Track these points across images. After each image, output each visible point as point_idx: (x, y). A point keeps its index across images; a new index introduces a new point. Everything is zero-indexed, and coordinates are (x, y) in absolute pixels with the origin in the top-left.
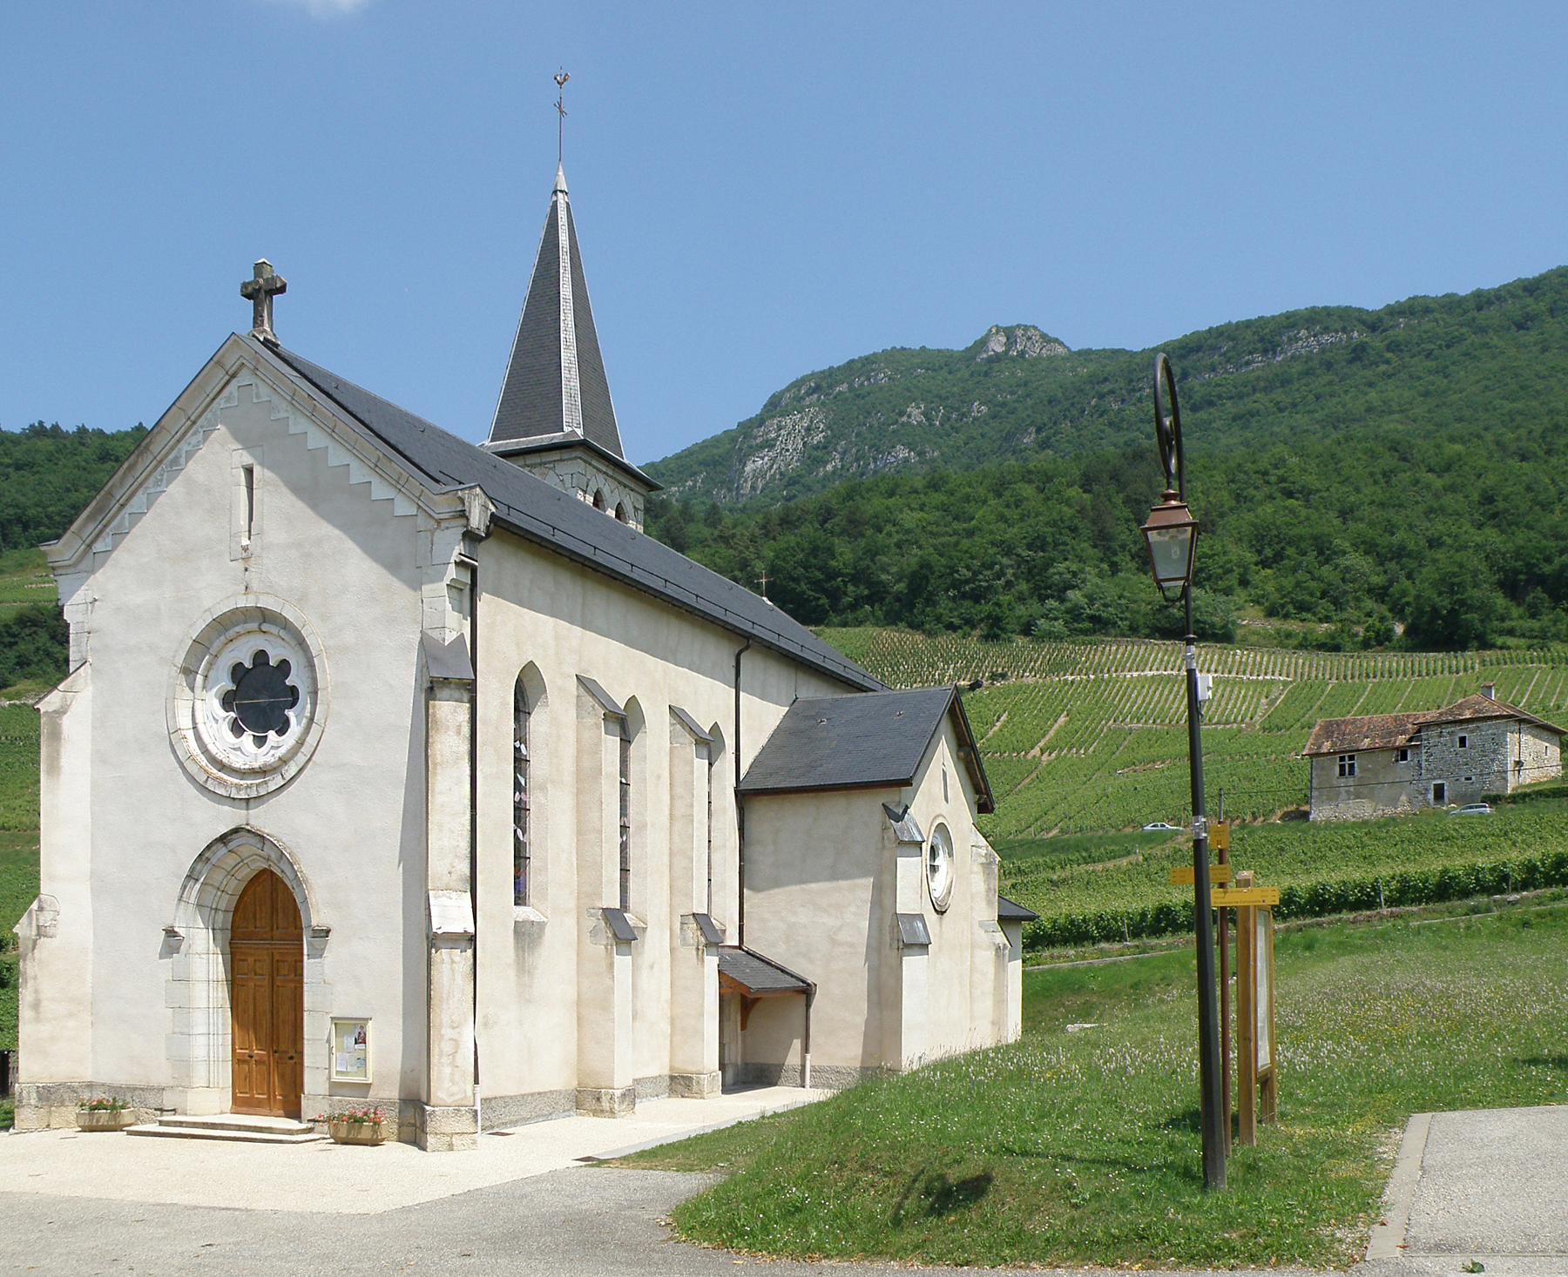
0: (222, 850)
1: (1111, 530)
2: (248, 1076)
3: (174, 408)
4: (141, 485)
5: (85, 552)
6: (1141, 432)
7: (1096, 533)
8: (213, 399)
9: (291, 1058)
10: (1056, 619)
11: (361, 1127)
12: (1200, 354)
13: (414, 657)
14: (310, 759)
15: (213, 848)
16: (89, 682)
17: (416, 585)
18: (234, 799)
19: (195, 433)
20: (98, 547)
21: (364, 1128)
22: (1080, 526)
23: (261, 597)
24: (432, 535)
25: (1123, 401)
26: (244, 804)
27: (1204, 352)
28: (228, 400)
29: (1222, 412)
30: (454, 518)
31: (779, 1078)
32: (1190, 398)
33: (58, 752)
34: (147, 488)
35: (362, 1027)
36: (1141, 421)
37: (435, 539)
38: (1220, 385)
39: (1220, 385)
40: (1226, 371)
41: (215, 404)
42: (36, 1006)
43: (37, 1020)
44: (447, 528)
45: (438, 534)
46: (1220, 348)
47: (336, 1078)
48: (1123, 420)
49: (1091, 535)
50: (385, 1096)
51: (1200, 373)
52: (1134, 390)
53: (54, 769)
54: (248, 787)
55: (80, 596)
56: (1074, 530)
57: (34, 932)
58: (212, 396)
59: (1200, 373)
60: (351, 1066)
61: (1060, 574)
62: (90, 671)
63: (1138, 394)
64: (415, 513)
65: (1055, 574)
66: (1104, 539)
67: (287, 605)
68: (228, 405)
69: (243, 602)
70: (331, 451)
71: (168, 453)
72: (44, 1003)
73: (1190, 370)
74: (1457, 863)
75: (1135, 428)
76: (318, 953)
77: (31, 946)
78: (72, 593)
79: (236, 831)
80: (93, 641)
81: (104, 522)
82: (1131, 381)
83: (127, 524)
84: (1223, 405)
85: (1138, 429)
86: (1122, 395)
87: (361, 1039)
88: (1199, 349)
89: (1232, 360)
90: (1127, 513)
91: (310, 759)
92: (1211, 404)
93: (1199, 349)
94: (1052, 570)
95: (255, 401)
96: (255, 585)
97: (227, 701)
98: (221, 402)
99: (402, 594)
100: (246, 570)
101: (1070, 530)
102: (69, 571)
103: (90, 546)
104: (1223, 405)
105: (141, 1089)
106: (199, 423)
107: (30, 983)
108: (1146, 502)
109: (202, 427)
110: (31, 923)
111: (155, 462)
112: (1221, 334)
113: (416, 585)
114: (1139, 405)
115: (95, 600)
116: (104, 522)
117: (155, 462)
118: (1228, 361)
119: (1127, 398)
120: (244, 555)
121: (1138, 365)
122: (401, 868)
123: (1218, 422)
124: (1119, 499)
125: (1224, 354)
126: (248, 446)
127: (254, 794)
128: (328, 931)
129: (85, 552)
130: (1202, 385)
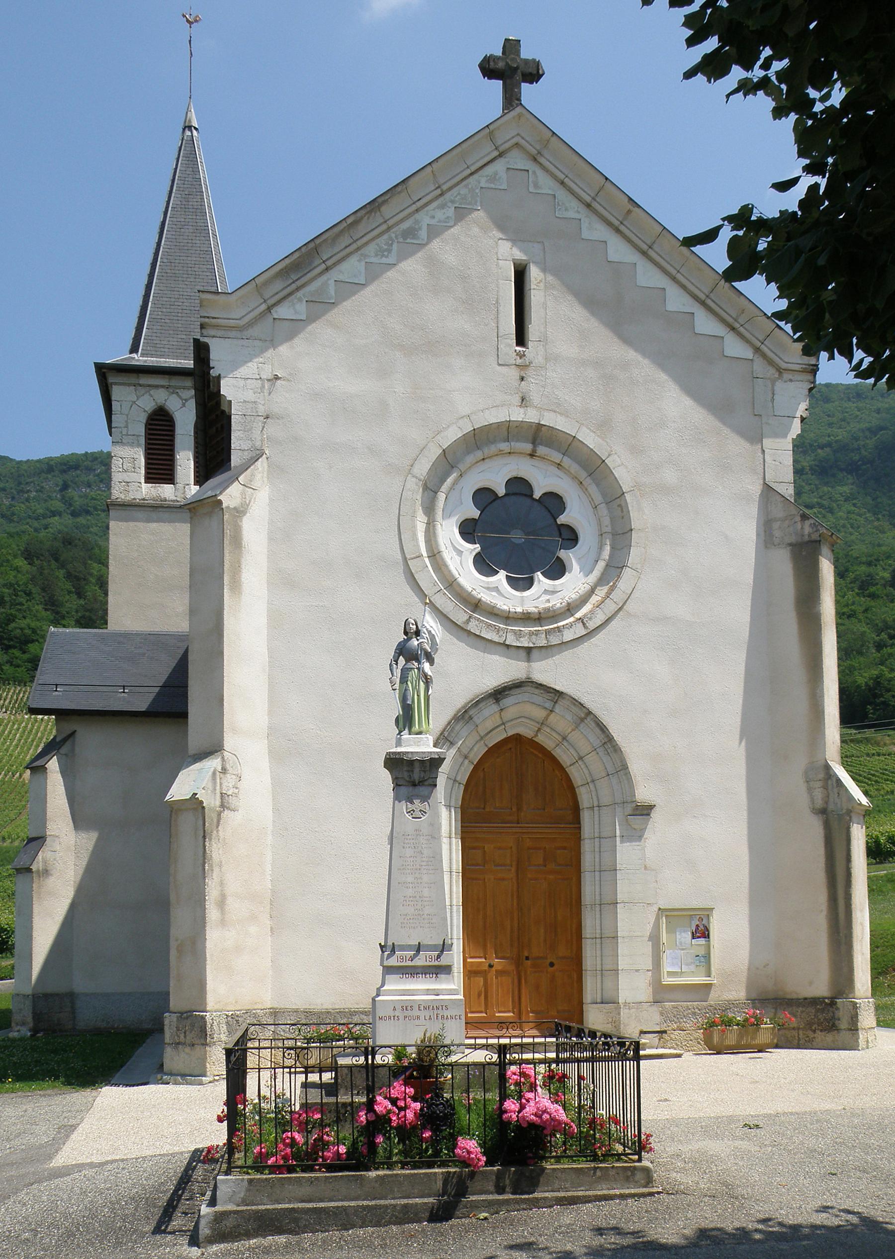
0: (491, 709)
1: (60, 598)
2: (486, 993)
3: (429, 169)
4: (359, 249)
5: (262, 315)
6: (30, 526)
7: (47, 598)
8: (472, 174)
9: (552, 965)
10: (18, 666)
11: (758, 1030)
12: (78, 472)
13: (754, 509)
14: (620, 609)
15: (481, 705)
16: (265, 479)
17: (755, 437)
18: (508, 646)
19: (442, 206)
20: (282, 312)
21: (761, 1032)
22: (34, 591)
23: (546, 414)
24: (773, 385)
25: (13, 498)
26: (523, 654)
27: (81, 471)
28: (493, 178)
29: (98, 520)
30: (804, 371)
31: (144, 1042)
32: (71, 505)
33: (239, 562)
34: (366, 256)
35: (701, 919)
36: (30, 517)
37: (775, 388)
38: (95, 499)
39: (95, 499)
40: (100, 489)
41: (472, 180)
42: (222, 903)
43: (223, 923)
44: (791, 380)
45: (779, 385)
46: (95, 470)
47: (667, 980)
48: (13, 514)
49: (43, 600)
50: (731, 997)
51: (78, 487)
52: (22, 491)
53: (236, 586)
54: (531, 634)
55: (250, 369)
56: (29, 594)
57: (218, 803)
58: (473, 168)
59: (78, 487)
60: (687, 965)
61: (22, 629)
62: (265, 465)
63: (26, 495)
64: (751, 358)
65: (16, 628)
66: (53, 604)
67: (584, 429)
68: (492, 186)
69: (518, 415)
70: (640, 268)
71: (402, 221)
72: (230, 900)
73: (70, 483)
74: (500, 868)
75: (25, 522)
76: (635, 835)
77: (215, 820)
78: (236, 366)
79: (518, 685)
80: (272, 429)
81: (299, 283)
82: (20, 483)
83: (332, 292)
84: (99, 515)
85: (28, 523)
86: (12, 493)
87: (703, 933)
88: (76, 467)
89: (104, 481)
90: (69, 586)
91: (620, 609)
92: (88, 512)
93: (76, 467)
94: (13, 625)
95: (531, 189)
96: (535, 397)
97: (468, 530)
98: (481, 180)
99: (737, 445)
100: (522, 379)
101: (25, 593)
102: (233, 334)
103: (269, 309)
104: (99, 515)
105: (362, 1013)
106: (448, 196)
107: (216, 870)
108: (85, 579)
109: (453, 202)
110: (215, 789)
111: (384, 227)
112: (95, 459)
113: (755, 437)
114: (27, 504)
115: (277, 378)
116: (299, 283)
117: (384, 227)
118: (101, 481)
119: (17, 496)
120: (519, 361)
121: (26, 472)
122: (743, 743)
123: (95, 528)
124: (61, 573)
125: (98, 475)
126: (516, 238)
127: (543, 643)
128: (651, 807)
129: (262, 315)
130: (80, 497)
